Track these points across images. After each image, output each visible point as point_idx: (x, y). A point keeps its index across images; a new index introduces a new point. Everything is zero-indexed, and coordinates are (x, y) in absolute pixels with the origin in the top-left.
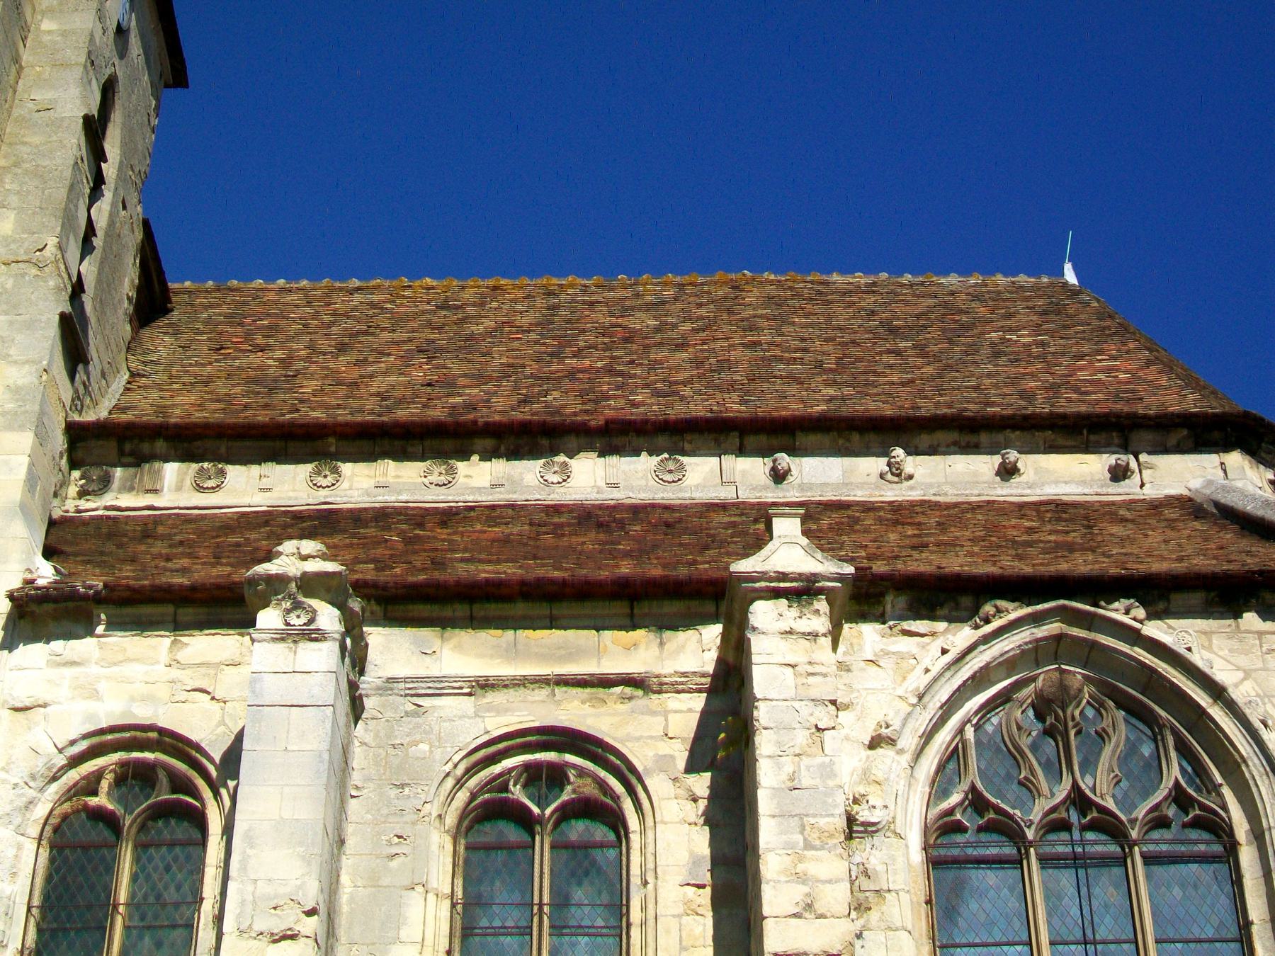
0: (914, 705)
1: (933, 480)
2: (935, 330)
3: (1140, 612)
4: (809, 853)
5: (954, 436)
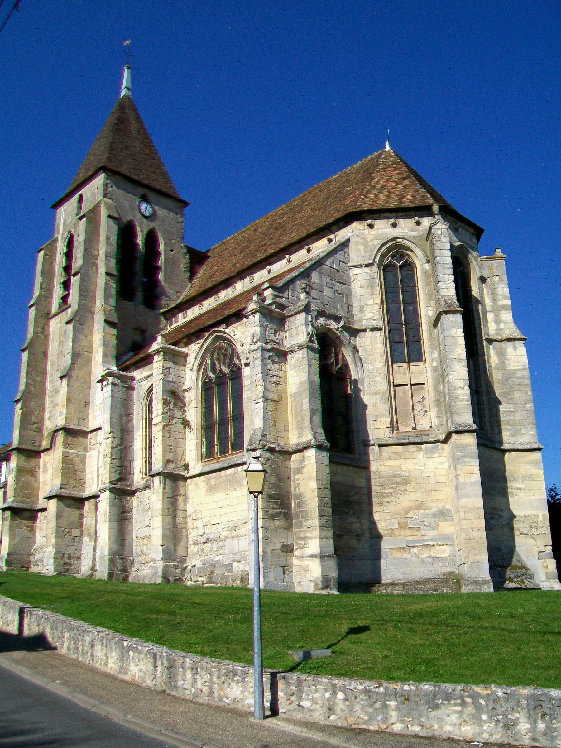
5: (297, 246)
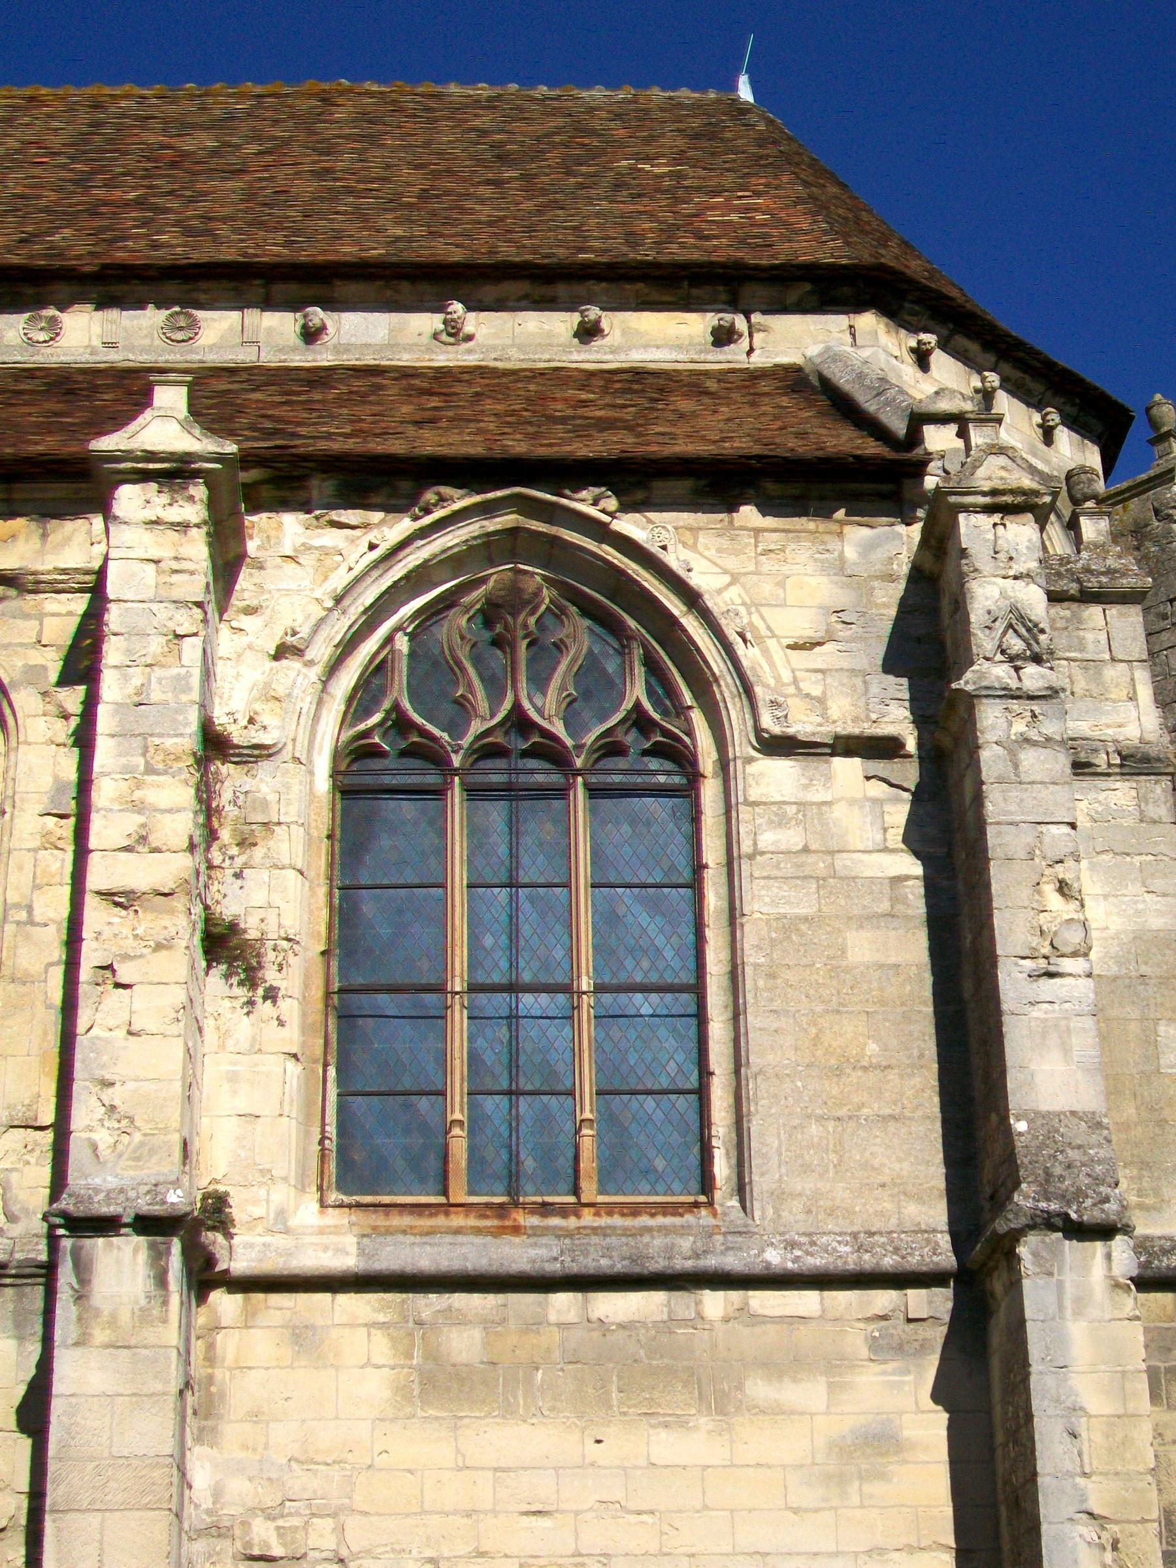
0: (330, 610)
1: (498, 342)
2: (554, 157)
3: (612, 503)
4: (150, 779)
5: (524, 287)
